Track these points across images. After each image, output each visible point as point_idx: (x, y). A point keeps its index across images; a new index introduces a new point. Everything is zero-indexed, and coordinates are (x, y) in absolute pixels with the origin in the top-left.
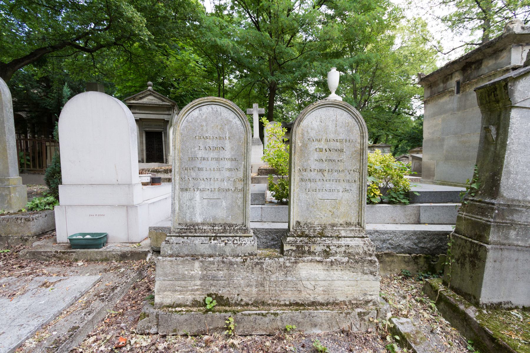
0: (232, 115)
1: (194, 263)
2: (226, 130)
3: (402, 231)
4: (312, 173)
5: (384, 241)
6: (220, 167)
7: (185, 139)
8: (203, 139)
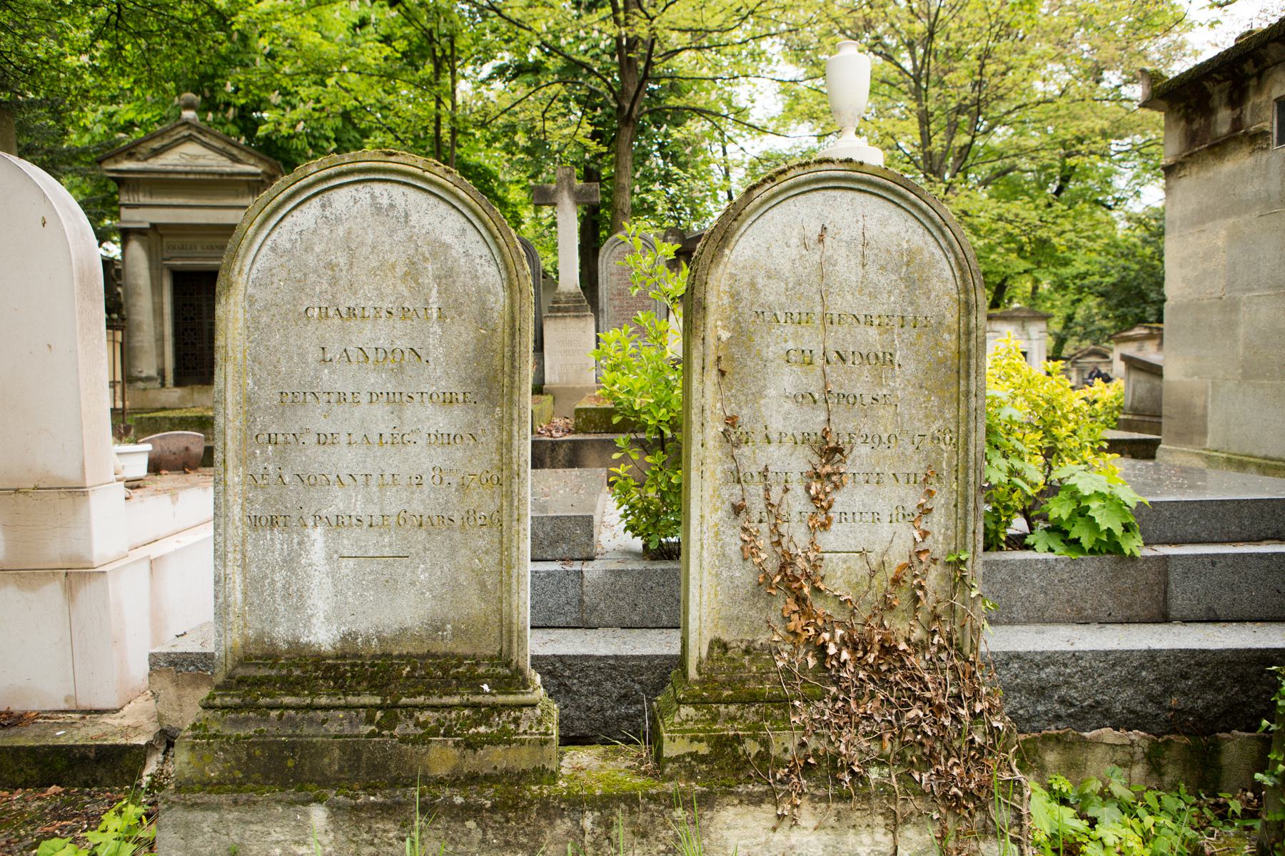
0: (454, 221)
1: (307, 815)
2: (428, 280)
3: (1107, 653)
4: (772, 448)
5: (1041, 692)
6: (406, 429)
7: (265, 319)
8: (337, 321)
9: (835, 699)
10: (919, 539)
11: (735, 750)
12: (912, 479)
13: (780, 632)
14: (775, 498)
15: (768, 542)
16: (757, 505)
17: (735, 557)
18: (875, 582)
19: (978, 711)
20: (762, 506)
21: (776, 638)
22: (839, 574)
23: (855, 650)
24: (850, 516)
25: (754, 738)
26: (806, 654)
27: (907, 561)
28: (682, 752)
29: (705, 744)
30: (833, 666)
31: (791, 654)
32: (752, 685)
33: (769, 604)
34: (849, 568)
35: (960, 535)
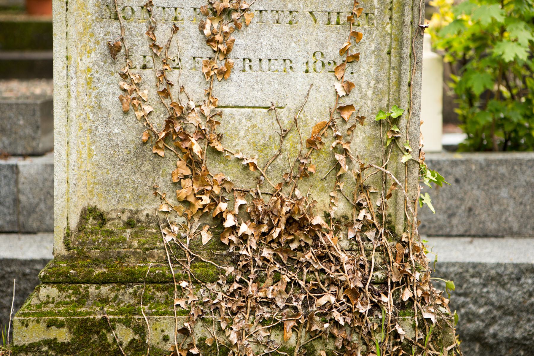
9: (230, 281)
10: (342, 93)
11: (103, 338)
12: (334, 18)
13: (170, 201)
14: (161, 41)
15: (154, 92)
16: (140, 48)
17: (115, 111)
18: (287, 144)
19: (406, 298)
20: (146, 48)
21: (165, 208)
22: (242, 133)
23: (260, 223)
24: (255, 63)
25: (127, 323)
26: (200, 228)
27: (327, 119)
28: (37, 340)
29: (65, 330)
30: (231, 242)
31: (183, 228)
32: (133, 263)
33: (156, 168)
34: (254, 126)
35: (394, 88)
